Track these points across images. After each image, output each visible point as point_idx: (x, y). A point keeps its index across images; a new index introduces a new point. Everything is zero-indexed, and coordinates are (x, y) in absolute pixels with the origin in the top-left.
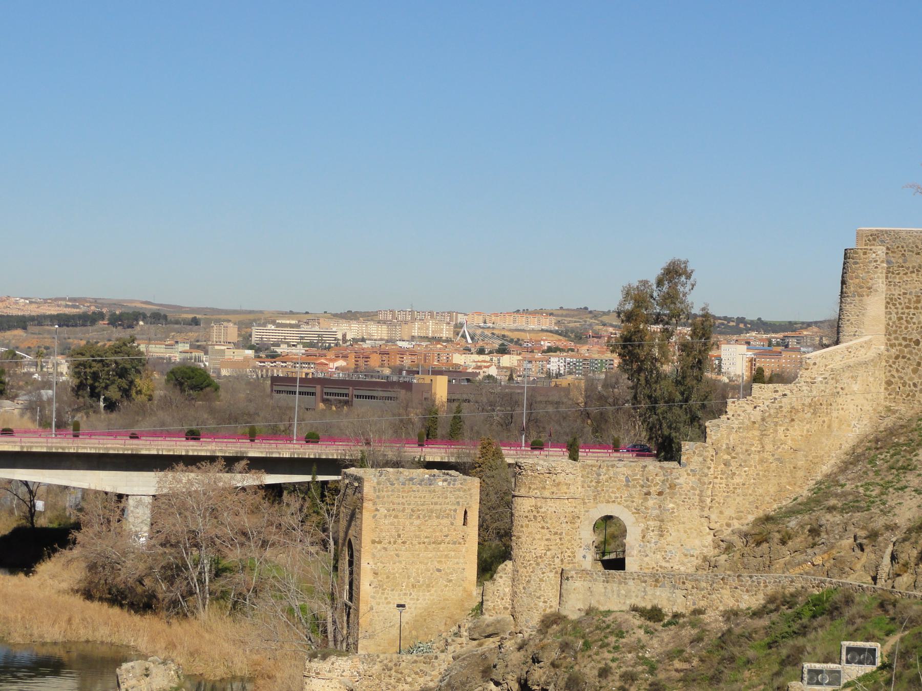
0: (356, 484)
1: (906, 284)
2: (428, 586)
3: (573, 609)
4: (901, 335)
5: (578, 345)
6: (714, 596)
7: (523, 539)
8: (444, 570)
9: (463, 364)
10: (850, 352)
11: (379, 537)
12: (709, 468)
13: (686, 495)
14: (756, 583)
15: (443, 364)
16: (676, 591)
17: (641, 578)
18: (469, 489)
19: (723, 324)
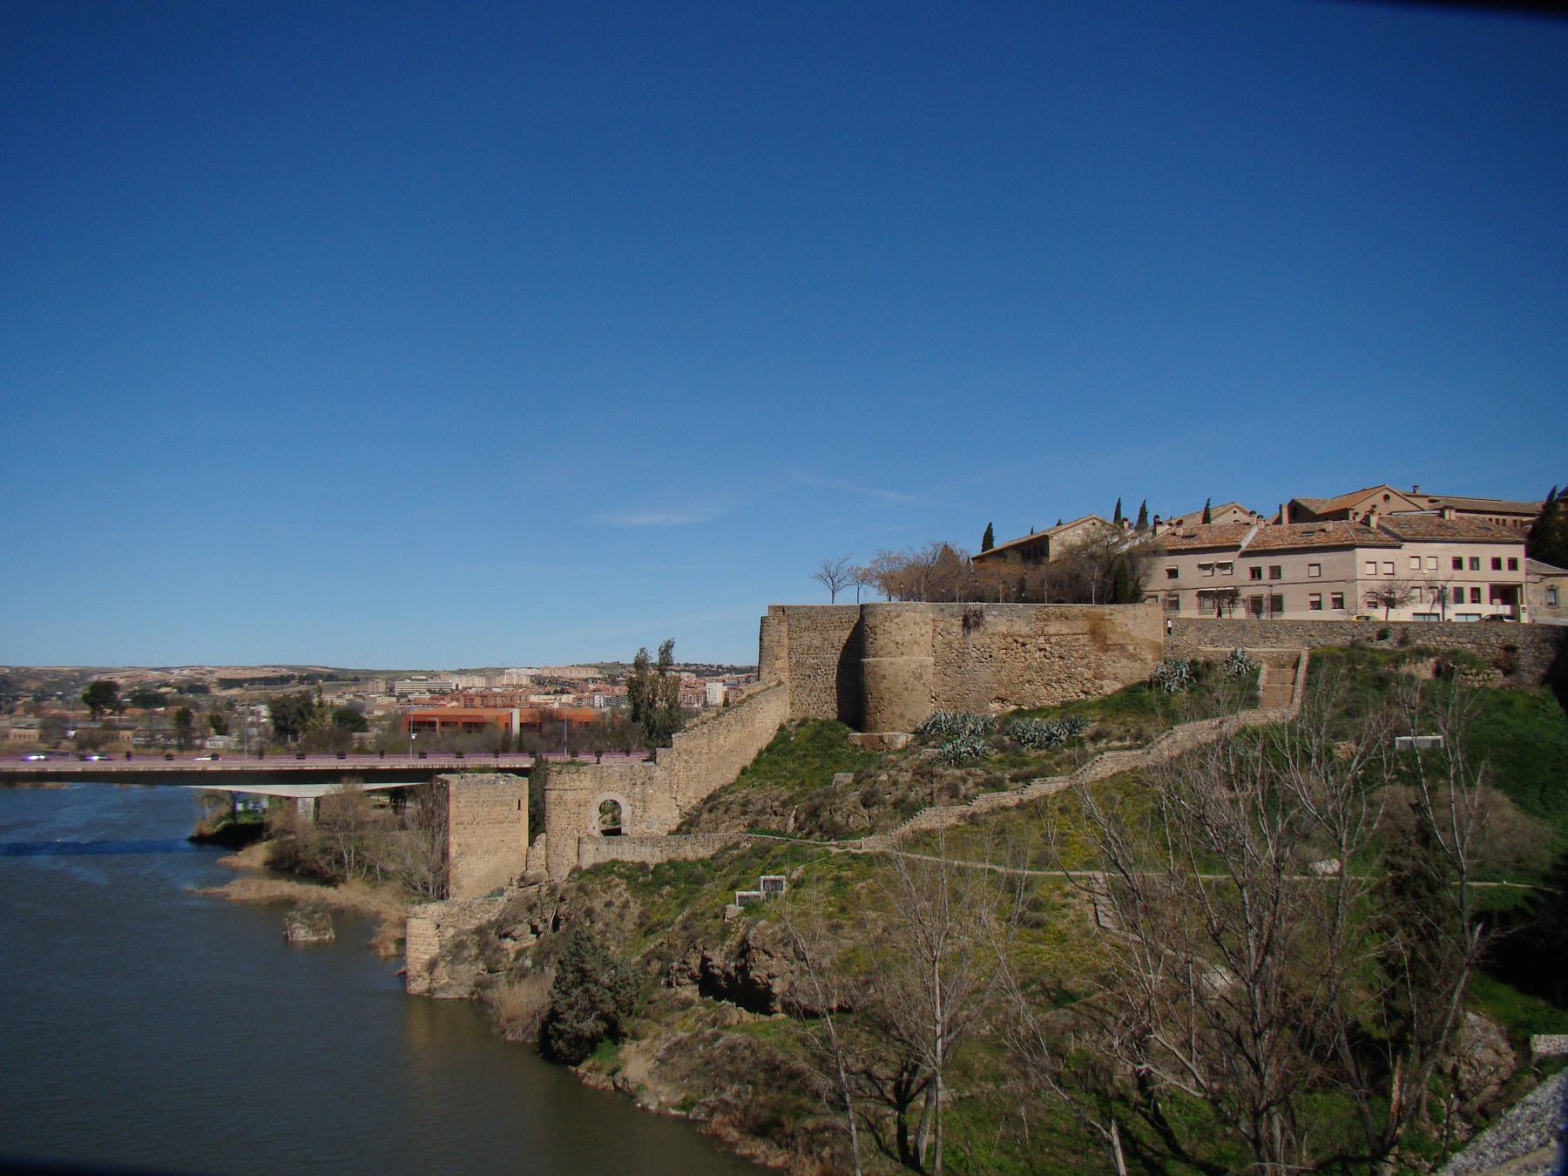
3: (587, 861)
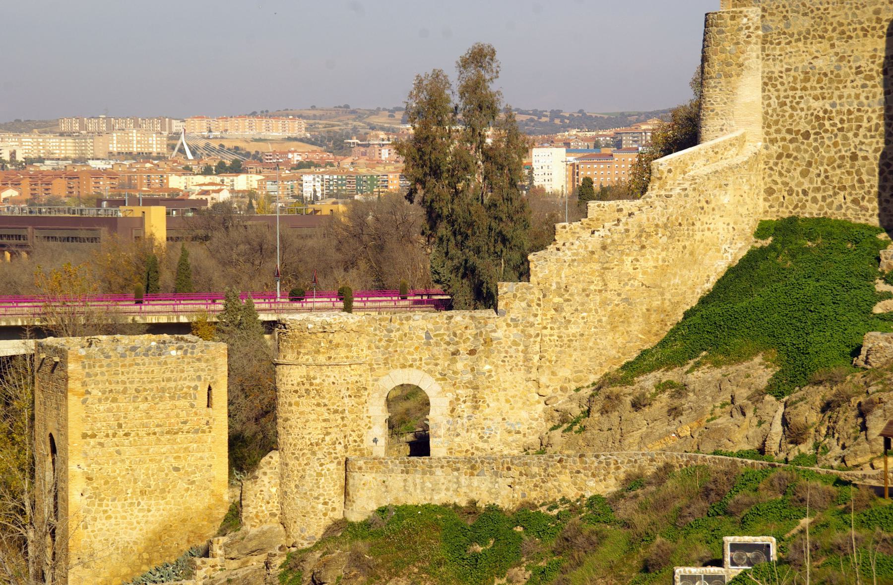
0: (57, 359)
1: (790, 57)
2: (163, 491)
4: (784, 126)
5: (338, 157)
6: (549, 484)
7: (292, 422)
8: (183, 468)
9: (183, 188)
10: (717, 153)
11: (92, 429)
12: (536, 316)
13: (507, 352)
14: (604, 465)
15: (155, 189)
16: (499, 480)
17: (452, 465)
18: (214, 359)
19: (532, 120)
